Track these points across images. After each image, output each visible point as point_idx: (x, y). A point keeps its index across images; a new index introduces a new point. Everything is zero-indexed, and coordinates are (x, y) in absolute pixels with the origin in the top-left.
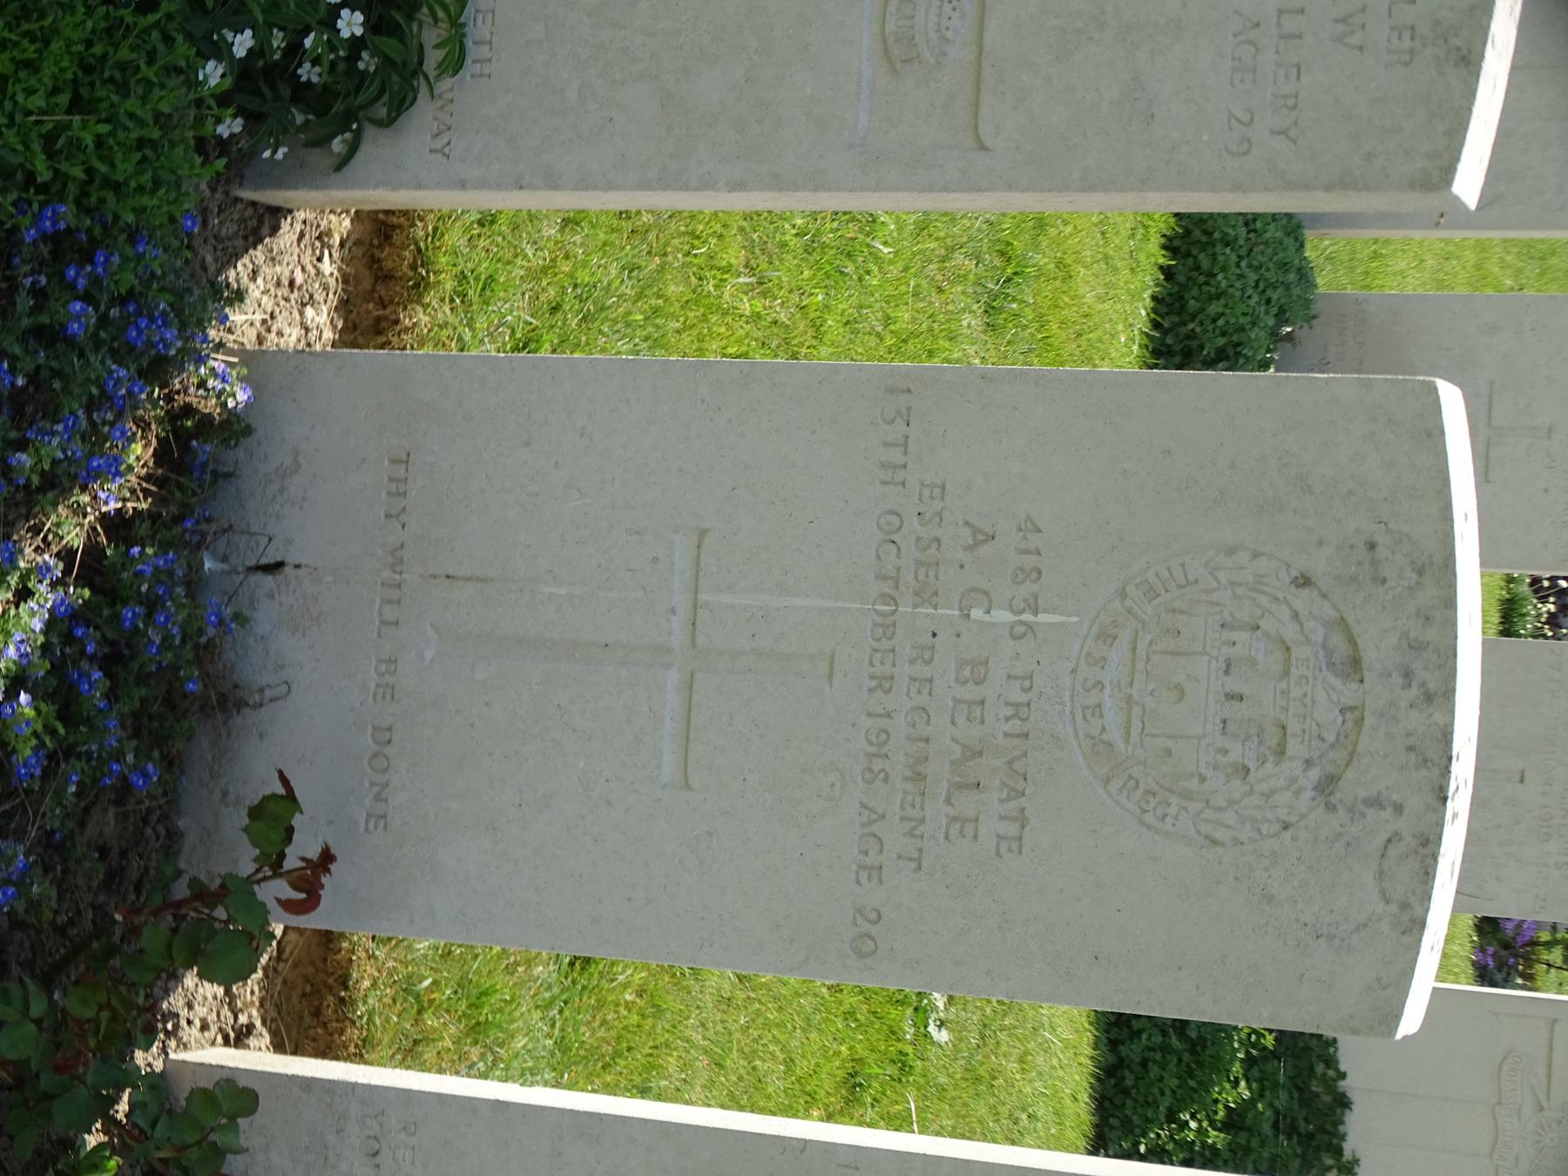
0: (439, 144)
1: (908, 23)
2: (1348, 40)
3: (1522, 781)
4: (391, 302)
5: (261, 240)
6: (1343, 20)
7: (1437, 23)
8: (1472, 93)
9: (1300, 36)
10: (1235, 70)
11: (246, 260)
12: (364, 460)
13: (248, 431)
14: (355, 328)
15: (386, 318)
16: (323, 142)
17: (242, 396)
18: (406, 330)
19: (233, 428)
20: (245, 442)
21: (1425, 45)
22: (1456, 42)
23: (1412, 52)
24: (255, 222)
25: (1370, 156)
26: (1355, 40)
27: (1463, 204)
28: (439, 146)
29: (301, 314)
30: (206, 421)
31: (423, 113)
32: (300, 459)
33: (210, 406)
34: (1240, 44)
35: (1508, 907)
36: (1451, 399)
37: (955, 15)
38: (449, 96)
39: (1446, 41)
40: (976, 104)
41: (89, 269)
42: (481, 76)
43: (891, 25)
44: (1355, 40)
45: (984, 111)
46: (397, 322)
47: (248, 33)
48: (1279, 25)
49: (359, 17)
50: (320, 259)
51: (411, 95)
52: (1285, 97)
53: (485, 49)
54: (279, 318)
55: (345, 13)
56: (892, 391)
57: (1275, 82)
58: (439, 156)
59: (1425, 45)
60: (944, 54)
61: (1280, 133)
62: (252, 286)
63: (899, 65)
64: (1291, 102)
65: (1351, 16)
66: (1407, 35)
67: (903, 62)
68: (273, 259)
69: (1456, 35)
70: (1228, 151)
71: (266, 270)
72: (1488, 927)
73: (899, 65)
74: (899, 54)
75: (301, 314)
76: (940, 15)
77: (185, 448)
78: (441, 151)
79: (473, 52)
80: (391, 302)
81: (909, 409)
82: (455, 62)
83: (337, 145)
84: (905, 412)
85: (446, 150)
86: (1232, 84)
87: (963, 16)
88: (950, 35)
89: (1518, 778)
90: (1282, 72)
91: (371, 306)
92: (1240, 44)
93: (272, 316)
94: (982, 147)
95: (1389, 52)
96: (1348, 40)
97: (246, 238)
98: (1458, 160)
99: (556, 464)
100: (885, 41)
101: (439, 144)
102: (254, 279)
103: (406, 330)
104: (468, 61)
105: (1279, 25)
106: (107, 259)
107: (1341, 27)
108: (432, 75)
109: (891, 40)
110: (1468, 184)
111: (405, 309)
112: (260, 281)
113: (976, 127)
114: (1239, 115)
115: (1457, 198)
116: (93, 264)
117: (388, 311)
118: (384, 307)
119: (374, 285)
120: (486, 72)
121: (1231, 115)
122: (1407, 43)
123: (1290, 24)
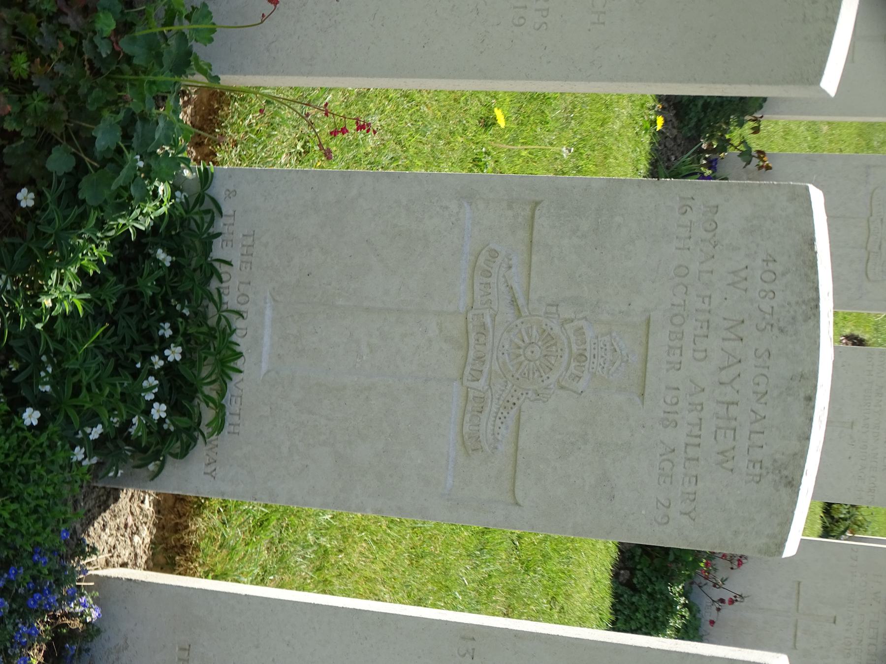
0: (209, 470)
1: (476, 428)
2: (724, 465)
3: (835, 622)
4: (185, 515)
5: (108, 507)
6: (722, 453)
7: (775, 461)
8: (794, 503)
9: (698, 460)
10: (660, 475)
11: (100, 519)
12: (164, 646)
13: (99, 631)
14: (164, 527)
15: (181, 524)
16: (144, 465)
17: (95, 614)
18: (193, 532)
19: (92, 631)
20: (96, 639)
21: (768, 473)
22: (785, 473)
23: (761, 475)
24: (105, 497)
25: (736, 533)
26: (729, 465)
27: (828, 95)
28: (209, 471)
29: (131, 540)
30: (73, 633)
31: (200, 451)
32: (128, 642)
33: (76, 624)
34: (664, 460)
35: (841, 497)
36: (817, 197)
37: (503, 427)
38: (215, 443)
39: (780, 471)
40: (514, 478)
41: (6, 576)
42: (234, 433)
43: (466, 429)
44: (729, 465)
45: (518, 483)
46: (187, 527)
47: (100, 426)
48: (685, 452)
49: (164, 407)
50: (143, 502)
51: (193, 443)
52: (688, 493)
53: (236, 418)
54: (119, 547)
55: (156, 405)
56: (463, 638)
57: (683, 484)
58: (209, 477)
59: (768, 473)
60: (496, 448)
61: (685, 514)
62: (103, 534)
63: (470, 452)
64: (692, 497)
65: (726, 451)
66: (758, 466)
67: (473, 450)
68: (115, 516)
69: (786, 469)
70: (655, 520)
71: (112, 524)
72: (828, 508)
73: (470, 452)
74: (471, 445)
75: (131, 540)
76: (494, 426)
77: (61, 649)
78: (210, 474)
79: (229, 419)
80: (185, 515)
81: (473, 649)
82: (219, 425)
83: (152, 467)
84: (471, 651)
85: (214, 474)
86: (668, 354)
87: (507, 428)
88: (499, 437)
89: (832, 620)
90: (687, 479)
91: (172, 516)
92: (664, 460)
93: (114, 547)
94: (517, 504)
95: (747, 474)
96: (724, 465)
97: (100, 507)
98: (786, 540)
99: (273, 660)
100: (463, 437)
101: (209, 470)
102: (104, 530)
103: (193, 532)
104: (227, 424)
105: (685, 452)
106: (16, 572)
107: (721, 457)
108: (206, 431)
109: (466, 437)
110: (831, 81)
111: (192, 519)
112: (107, 530)
113: (514, 491)
114: (663, 501)
115: (824, 91)
116: (9, 574)
117: (182, 521)
118: (180, 517)
119: (175, 504)
120: (236, 431)
121: (658, 501)
122: (757, 470)
123: (692, 452)
